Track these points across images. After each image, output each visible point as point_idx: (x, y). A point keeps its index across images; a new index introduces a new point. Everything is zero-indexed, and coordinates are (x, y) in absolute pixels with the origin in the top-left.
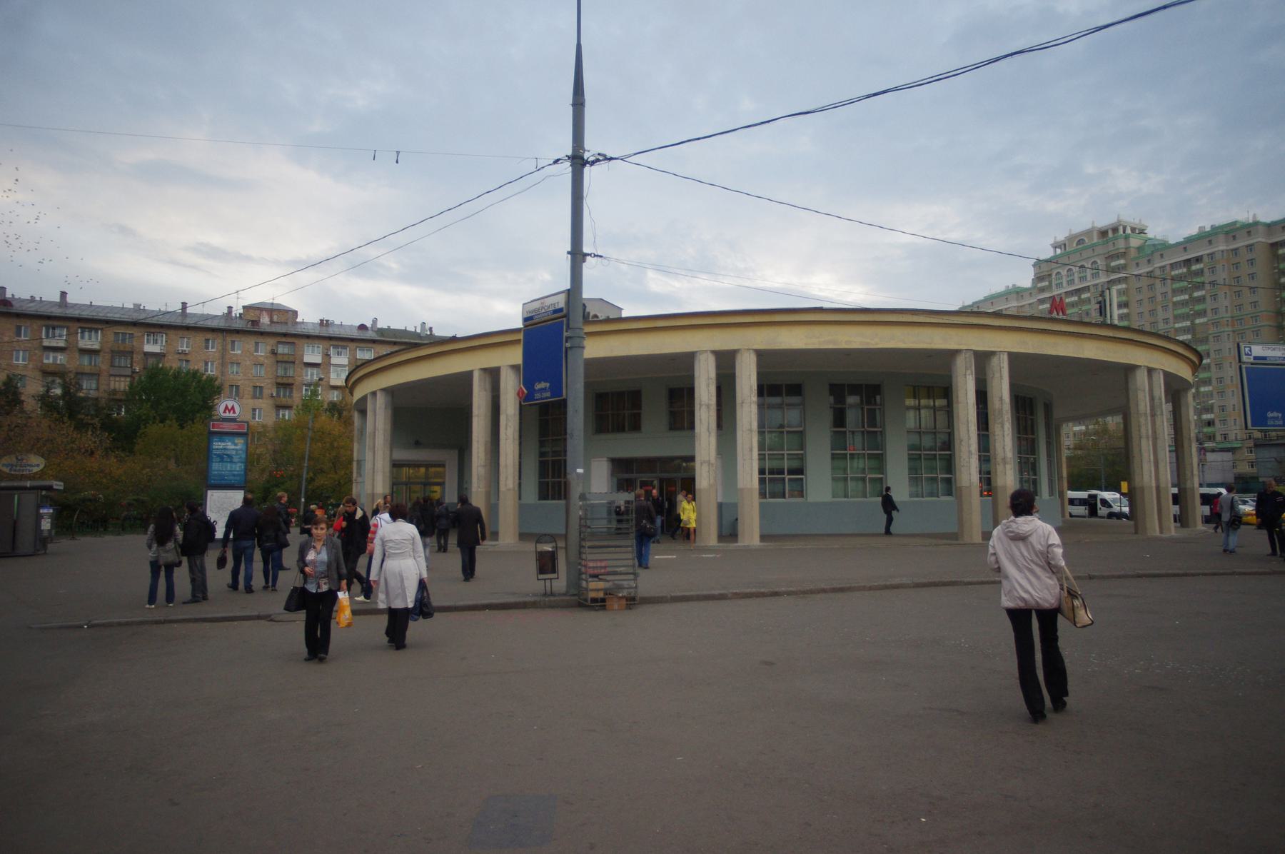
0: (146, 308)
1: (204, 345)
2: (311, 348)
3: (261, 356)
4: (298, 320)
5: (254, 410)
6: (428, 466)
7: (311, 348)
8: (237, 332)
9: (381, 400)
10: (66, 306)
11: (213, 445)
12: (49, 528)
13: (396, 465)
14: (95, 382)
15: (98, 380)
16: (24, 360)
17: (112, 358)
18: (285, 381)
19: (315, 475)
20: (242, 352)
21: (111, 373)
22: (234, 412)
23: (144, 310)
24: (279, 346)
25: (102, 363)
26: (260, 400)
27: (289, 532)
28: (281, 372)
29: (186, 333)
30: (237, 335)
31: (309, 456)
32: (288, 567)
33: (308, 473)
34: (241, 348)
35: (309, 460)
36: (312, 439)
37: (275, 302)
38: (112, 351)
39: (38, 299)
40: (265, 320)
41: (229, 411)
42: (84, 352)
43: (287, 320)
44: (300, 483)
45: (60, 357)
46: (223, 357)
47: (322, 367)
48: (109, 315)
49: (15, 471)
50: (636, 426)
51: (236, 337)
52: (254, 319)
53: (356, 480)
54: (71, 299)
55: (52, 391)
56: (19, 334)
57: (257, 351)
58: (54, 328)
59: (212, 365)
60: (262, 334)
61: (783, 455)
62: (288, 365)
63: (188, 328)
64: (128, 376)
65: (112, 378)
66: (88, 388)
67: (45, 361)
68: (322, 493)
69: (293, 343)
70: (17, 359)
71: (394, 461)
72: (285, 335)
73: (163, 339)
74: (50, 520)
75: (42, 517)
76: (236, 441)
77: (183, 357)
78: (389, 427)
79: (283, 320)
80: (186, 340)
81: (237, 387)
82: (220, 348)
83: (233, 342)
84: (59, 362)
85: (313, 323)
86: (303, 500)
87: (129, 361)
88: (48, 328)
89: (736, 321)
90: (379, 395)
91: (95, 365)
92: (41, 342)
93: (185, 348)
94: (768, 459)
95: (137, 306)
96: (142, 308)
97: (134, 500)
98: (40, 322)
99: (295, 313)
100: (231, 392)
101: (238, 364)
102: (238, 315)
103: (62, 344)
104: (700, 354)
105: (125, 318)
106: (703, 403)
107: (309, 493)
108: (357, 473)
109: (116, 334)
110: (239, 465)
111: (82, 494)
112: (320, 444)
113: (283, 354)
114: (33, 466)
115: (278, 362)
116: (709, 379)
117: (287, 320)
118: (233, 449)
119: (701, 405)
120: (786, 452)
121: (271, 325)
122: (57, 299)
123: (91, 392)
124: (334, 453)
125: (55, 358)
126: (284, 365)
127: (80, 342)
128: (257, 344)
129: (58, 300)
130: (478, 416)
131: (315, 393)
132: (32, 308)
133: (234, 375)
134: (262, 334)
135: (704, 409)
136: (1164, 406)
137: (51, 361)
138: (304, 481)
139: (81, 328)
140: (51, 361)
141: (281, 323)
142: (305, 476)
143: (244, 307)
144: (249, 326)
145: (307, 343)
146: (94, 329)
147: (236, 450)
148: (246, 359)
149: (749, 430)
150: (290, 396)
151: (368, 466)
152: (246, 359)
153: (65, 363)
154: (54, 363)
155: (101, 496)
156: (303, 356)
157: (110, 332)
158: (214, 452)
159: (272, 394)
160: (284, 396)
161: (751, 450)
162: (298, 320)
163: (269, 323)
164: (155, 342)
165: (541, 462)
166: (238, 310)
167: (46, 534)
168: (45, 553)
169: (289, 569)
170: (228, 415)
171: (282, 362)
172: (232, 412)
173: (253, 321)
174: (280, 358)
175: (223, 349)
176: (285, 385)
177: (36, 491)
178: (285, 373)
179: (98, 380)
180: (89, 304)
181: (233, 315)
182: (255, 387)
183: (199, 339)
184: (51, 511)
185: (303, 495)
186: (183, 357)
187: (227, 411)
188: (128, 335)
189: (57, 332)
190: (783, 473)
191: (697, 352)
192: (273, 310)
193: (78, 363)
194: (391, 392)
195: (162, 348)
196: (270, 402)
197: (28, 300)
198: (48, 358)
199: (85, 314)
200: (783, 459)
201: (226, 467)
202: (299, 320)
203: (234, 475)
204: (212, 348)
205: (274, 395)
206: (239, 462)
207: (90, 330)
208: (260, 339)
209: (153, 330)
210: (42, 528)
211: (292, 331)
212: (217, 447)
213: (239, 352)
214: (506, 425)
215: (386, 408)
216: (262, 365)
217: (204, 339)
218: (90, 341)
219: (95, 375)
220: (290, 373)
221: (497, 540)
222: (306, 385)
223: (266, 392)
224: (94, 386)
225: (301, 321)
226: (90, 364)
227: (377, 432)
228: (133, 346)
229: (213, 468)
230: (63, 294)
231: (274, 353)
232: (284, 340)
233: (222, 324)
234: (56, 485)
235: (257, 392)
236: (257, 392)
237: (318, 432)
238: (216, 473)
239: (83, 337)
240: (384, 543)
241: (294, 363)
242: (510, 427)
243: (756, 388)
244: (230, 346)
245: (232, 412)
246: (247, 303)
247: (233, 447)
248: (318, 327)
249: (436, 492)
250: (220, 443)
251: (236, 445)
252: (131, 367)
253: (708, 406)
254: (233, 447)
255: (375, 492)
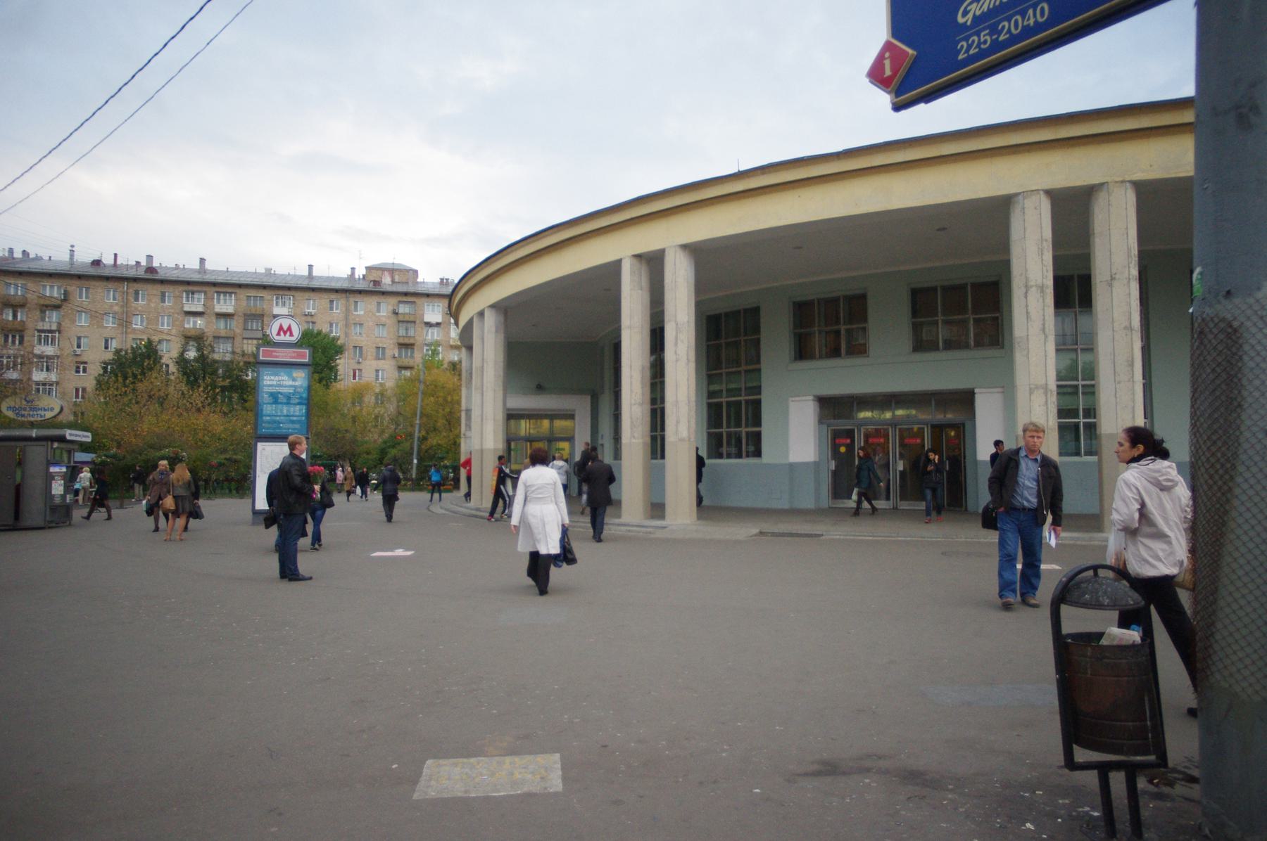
0: (276, 273)
1: (329, 306)
2: (431, 307)
3: (383, 316)
4: (419, 280)
5: (377, 371)
6: (552, 416)
7: (431, 307)
8: (360, 292)
9: (491, 319)
10: (205, 272)
11: (263, 379)
12: (62, 493)
13: (512, 416)
14: (230, 345)
15: (233, 344)
16: (168, 325)
17: (245, 322)
18: (406, 341)
19: (428, 433)
20: (365, 313)
21: (244, 336)
22: (291, 335)
23: (275, 274)
24: (401, 305)
25: (236, 325)
26: (383, 361)
27: (331, 505)
28: (402, 332)
29: (312, 295)
30: (359, 296)
31: (421, 413)
32: (307, 575)
33: (420, 432)
34: (364, 308)
35: (421, 417)
36: (424, 393)
37: (396, 262)
38: (245, 315)
39: (181, 267)
40: (387, 280)
41: (285, 333)
42: (221, 316)
43: (408, 279)
44: (412, 444)
45: (199, 322)
46: (347, 318)
47: (442, 326)
48: (242, 279)
49: (23, 416)
50: (858, 350)
51: (358, 298)
52: (377, 280)
53: (464, 435)
54: (209, 266)
55: (187, 353)
56: (163, 301)
57: (378, 311)
58: (193, 293)
59: (337, 326)
60: (384, 293)
61: (1076, 387)
62: (409, 325)
63: (313, 290)
64: (259, 339)
65: (245, 341)
66: (222, 352)
67: (187, 326)
68: (436, 453)
69: (415, 302)
70: (163, 325)
71: (508, 410)
72: (406, 294)
73: (290, 302)
74: (62, 482)
75: (53, 478)
76: (295, 375)
77: (309, 319)
78: (501, 357)
79: (404, 280)
80: (312, 302)
81: (361, 348)
82: (344, 309)
83: (356, 302)
84: (198, 327)
85: (433, 283)
86: (415, 461)
87: (260, 324)
88: (187, 292)
89: (1100, 131)
90: (487, 313)
91: (230, 329)
92: (183, 307)
93: (311, 310)
94: (1083, 393)
95: (268, 270)
96: (272, 272)
97: (226, 459)
98: (181, 288)
99: (416, 272)
100: (355, 352)
101: (361, 325)
102: (361, 277)
103: (200, 309)
104: (1024, 198)
105: (256, 281)
106: (1032, 283)
107: (422, 454)
108: (466, 425)
109: (249, 297)
110: (298, 407)
111: (162, 452)
112: (432, 398)
113: (404, 314)
114: (45, 410)
115: (399, 321)
116: (1042, 240)
117: (408, 279)
118: (291, 386)
119: (1027, 287)
120: (1081, 383)
121: (392, 285)
122: (197, 267)
123: (227, 355)
124: (448, 410)
125: (195, 323)
126: (405, 324)
127: (216, 307)
128: (379, 304)
129: (198, 267)
130: (630, 327)
131: (435, 353)
132: (174, 275)
133: (357, 337)
134: (384, 293)
135: (1034, 295)
136: (872, 427)
137: (191, 326)
138: (416, 440)
139: (217, 292)
140: (191, 325)
141: (403, 283)
142: (416, 434)
143: (367, 268)
144: (371, 286)
145: (427, 302)
146: (229, 293)
147: (295, 387)
148: (369, 319)
149: (1125, 328)
150: (412, 357)
151: (475, 414)
152: (369, 319)
153: (204, 328)
154: (195, 328)
155: (184, 454)
156: (423, 315)
157: (243, 294)
158: (266, 389)
159: (394, 355)
160: (406, 357)
161: (1132, 365)
162: (419, 280)
163: (390, 283)
164: (284, 305)
165: (710, 405)
166: (360, 272)
167: (58, 501)
168: (70, 525)
169: (310, 578)
170: (282, 338)
171: (403, 322)
172: (288, 333)
173: (374, 281)
174: (401, 318)
175: (346, 310)
176: (406, 346)
177: (44, 443)
178: (407, 333)
179: (233, 344)
180: (226, 269)
181: (357, 277)
182: (378, 348)
183: (323, 301)
184: (64, 469)
185: (415, 456)
186: (309, 319)
187: (282, 333)
188: (252, 298)
189: (196, 296)
190: (1077, 416)
191: (1017, 195)
192: (392, 270)
193: (215, 327)
194: (503, 308)
195: (290, 310)
196: (393, 362)
197: (172, 268)
198: (189, 323)
199: (220, 279)
200: (1076, 393)
201: (282, 411)
202: (420, 280)
203: (293, 422)
204: (336, 309)
205: (396, 355)
206: (299, 404)
207: (225, 293)
208: (382, 299)
209: (281, 293)
210: (53, 493)
211: (411, 289)
212: (268, 383)
213: (362, 313)
214: (676, 338)
215: (496, 331)
216: (383, 325)
217: (328, 300)
218: (226, 305)
219: (230, 338)
220: (411, 333)
221: (662, 517)
222: (427, 345)
223: (389, 353)
224: (230, 349)
225: (422, 281)
226: (226, 328)
227: (485, 365)
228: (263, 308)
229: (264, 412)
230: (202, 261)
231: (395, 313)
232: (405, 299)
233: (346, 285)
234: (71, 435)
235: (380, 352)
236: (380, 352)
237: (431, 385)
238: (268, 418)
239: (218, 302)
240: (526, 487)
241: (414, 322)
242: (682, 342)
243: (1136, 253)
244: (353, 307)
245: (288, 333)
246: (369, 264)
247: (291, 383)
248: (438, 286)
249: (563, 449)
250: (272, 378)
251: (294, 380)
252: (262, 330)
253: (1042, 289)
254: (291, 383)
255: (484, 447)
